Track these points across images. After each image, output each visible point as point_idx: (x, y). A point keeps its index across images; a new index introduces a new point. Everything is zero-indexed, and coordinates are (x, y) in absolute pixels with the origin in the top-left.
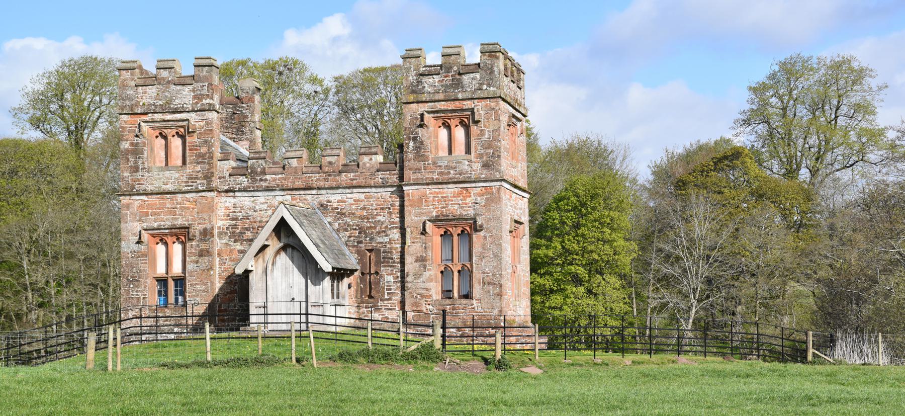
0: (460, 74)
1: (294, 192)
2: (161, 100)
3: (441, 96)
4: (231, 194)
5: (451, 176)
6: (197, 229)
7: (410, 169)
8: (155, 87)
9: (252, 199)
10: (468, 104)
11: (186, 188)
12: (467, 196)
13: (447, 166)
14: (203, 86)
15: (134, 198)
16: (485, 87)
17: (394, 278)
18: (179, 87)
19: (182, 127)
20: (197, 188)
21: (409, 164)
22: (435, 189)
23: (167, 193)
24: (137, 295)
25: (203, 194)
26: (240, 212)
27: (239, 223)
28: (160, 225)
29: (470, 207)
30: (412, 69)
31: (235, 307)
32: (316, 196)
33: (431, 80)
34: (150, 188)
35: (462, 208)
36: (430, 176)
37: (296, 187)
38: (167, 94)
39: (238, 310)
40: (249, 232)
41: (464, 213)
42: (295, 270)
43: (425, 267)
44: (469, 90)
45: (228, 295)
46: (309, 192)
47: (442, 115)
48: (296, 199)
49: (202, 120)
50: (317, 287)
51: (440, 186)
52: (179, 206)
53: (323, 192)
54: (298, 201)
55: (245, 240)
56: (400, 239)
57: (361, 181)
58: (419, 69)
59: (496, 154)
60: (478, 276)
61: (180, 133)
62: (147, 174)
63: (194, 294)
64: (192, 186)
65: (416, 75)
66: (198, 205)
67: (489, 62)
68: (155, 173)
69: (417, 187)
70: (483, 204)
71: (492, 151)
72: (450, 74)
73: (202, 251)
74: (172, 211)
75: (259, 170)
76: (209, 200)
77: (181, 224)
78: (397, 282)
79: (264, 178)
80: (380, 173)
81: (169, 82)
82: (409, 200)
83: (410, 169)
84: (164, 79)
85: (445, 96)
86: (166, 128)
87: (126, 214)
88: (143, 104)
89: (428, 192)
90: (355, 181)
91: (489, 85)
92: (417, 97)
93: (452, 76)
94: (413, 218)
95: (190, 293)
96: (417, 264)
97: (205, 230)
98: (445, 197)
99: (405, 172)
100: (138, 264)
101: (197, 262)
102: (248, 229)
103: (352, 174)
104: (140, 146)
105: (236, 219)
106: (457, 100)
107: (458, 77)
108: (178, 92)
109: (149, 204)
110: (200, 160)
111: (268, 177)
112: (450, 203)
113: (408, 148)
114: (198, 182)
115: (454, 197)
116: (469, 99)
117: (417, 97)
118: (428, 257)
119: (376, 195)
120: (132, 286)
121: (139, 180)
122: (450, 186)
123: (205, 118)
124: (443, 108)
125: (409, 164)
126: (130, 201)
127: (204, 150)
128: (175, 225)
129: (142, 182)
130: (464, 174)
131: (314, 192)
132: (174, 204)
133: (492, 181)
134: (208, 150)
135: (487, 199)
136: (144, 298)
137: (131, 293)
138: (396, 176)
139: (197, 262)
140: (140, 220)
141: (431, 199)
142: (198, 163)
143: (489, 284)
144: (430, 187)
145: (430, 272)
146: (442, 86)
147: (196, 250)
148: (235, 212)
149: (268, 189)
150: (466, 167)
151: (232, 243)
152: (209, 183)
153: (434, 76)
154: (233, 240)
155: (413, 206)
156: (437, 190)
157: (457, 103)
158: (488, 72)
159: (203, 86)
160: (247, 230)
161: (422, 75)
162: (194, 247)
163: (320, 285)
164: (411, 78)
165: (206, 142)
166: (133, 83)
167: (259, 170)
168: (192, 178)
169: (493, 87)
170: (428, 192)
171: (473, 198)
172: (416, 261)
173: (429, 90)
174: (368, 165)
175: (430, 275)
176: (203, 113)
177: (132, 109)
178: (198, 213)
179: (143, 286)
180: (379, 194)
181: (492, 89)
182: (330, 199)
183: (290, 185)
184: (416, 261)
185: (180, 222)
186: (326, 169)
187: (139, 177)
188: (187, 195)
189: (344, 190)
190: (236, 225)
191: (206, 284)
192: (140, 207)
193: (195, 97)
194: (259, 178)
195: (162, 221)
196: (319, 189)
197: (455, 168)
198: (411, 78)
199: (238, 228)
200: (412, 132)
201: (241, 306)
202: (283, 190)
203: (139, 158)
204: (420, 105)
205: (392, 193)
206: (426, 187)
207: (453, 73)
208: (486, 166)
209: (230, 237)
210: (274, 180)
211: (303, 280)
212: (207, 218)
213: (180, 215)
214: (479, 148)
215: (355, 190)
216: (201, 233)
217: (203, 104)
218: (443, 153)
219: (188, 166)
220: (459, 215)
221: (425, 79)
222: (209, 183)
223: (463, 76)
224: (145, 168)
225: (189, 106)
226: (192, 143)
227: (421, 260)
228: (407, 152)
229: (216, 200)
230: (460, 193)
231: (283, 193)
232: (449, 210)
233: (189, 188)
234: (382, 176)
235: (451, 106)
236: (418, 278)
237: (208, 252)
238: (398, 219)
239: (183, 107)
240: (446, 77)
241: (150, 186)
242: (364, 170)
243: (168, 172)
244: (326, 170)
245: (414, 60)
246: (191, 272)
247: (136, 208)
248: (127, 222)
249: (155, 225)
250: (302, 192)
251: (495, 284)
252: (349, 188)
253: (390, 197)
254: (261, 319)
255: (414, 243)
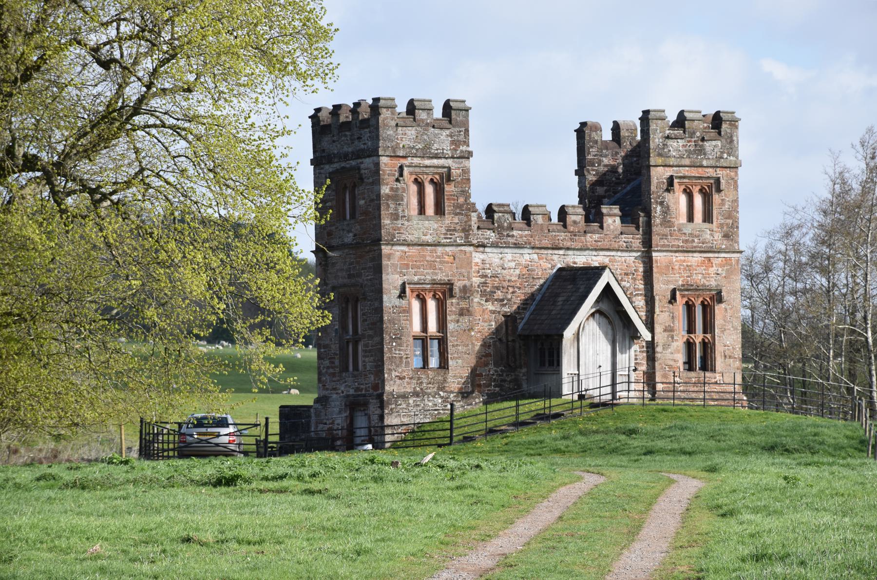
0: (703, 140)
1: (543, 251)
2: (419, 143)
3: (687, 162)
4: (481, 249)
5: (695, 244)
6: (458, 285)
7: (658, 235)
8: (414, 128)
9: (500, 256)
10: (711, 172)
11: (445, 241)
12: (709, 267)
13: (691, 234)
14: (460, 131)
15: (395, 248)
16: (725, 156)
17: (640, 347)
18: (437, 131)
19: (436, 173)
20: (455, 241)
21: (657, 229)
22: (681, 256)
23: (429, 245)
24: (399, 354)
25: (463, 248)
26: (490, 269)
27: (489, 280)
28: (420, 280)
29: (712, 277)
30: (658, 131)
31: (489, 371)
32: (563, 257)
33: (675, 144)
34: (410, 238)
35: (705, 278)
36: (676, 243)
37: (543, 246)
38: (425, 137)
39: (493, 375)
40: (499, 292)
41: (707, 283)
42: (602, 336)
43: (672, 337)
44: (711, 157)
45: (483, 359)
46: (556, 252)
47: (687, 181)
48: (542, 259)
49: (459, 169)
50: (624, 355)
51: (686, 254)
52: (438, 260)
53: (570, 252)
54: (545, 260)
55: (496, 300)
56: (644, 307)
57: (606, 244)
58: (664, 132)
59: (735, 224)
60: (720, 349)
61: (435, 180)
62: (406, 223)
63: (456, 355)
64: (451, 238)
65: (662, 137)
66: (457, 259)
67: (729, 131)
68: (415, 222)
69: (665, 254)
70: (724, 275)
71: (731, 221)
72: (693, 140)
73: (462, 309)
74: (432, 265)
75: (506, 224)
76: (468, 255)
77: (441, 280)
78: (643, 352)
79: (511, 233)
80: (623, 236)
81: (427, 124)
82: (657, 267)
83: (657, 234)
84: (423, 120)
85: (691, 162)
86: (423, 173)
87: (387, 265)
88: (403, 146)
89: (674, 260)
90: (600, 243)
91: (729, 154)
92: (665, 161)
93: (695, 141)
94: (661, 288)
95: (452, 354)
96: (666, 334)
97: (465, 287)
98: (690, 266)
99: (653, 238)
100: (400, 321)
101: (458, 321)
102: (498, 288)
103: (597, 235)
104: (400, 192)
105: (486, 276)
106: (702, 166)
107: (701, 143)
108: (436, 135)
109: (410, 256)
110: (458, 211)
111: (515, 233)
112: (695, 272)
113: (656, 213)
114: (457, 234)
115: (698, 266)
116: (711, 167)
117: (665, 161)
118: (676, 328)
119: (620, 259)
120: (394, 344)
121: (399, 229)
122: (695, 255)
123: (462, 165)
124: (687, 174)
125: (657, 229)
126: (391, 252)
127: (461, 200)
128: (434, 280)
129: (402, 231)
130: (707, 243)
131: (561, 252)
132: (433, 257)
133: (734, 252)
134: (466, 201)
135: (727, 270)
136: (407, 358)
137: (394, 351)
138: (639, 241)
139: (458, 321)
140: (401, 272)
141: (677, 267)
142: (456, 215)
143: (730, 357)
144: (677, 254)
145: (677, 343)
146: (686, 151)
147: (456, 308)
148: (484, 269)
149: (517, 246)
150: (708, 236)
151: (483, 302)
152: (467, 237)
153: (679, 140)
154: (484, 299)
155: (661, 273)
156: (683, 258)
157: (700, 170)
158: (728, 141)
159: (460, 131)
160: (498, 289)
161: (668, 137)
162: (454, 304)
163: (626, 353)
164: (657, 140)
165: (463, 191)
166: (393, 123)
167: (506, 224)
168: (450, 230)
169: (733, 156)
170: (674, 260)
171: (715, 268)
172: (665, 331)
173: (674, 154)
174: (612, 227)
175: (678, 346)
176: (461, 160)
177: (394, 152)
178: (457, 268)
179: (405, 345)
180: (623, 258)
181: (732, 158)
182: (576, 260)
183: (537, 244)
184: (665, 331)
185: (440, 277)
186: (572, 229)
187: (400, 226)
188: (448, 249)
189: (591, 252)
190: (486, 283)
191: (468, 345)
192: (401, 258)
193: (452, 143)
194: (505, 234)
195: (422, 275)
196: (568, 249)
197: (698, 236)
198: (657, 140)
199: (488, 287)
200: (659, 197)
201: (496, 371)
202: (533, 248)
203: (399, 204)
204: (667, 169)
205: (636, 259)
206: (673, 254)
207: (695, 139)
208: (726, 236)
209: (481, 296)
210: (521, 237)
211: (608, 349)
212: (466, 274)
213: (440, 269)
214: (720, 218)
215: (601, 253)
216: (460, 291)
217: (462, 151)
218: (683, 219)
219: (446, 216)
220: (702, 285)
221: (670, 142)
222: (467, 237)
223: (705, 143)
224: (405, 216)
225: (449, 152)
226: (449, 192)
227: (669, 330)
228: (655, 217)
229: (474, 254)
230: (703, 262)
231: (530, 251)
232: (694, 279)
233: (448, 241)
234: (626, 240)
235: (694, 172)
236: (667, 348)
237: (468, 311)
238: (643, 286)
239: (443, 153)
240: (689, 142)
241: (410, 236)
242: (608, 233)
243: (427, 222)
244: (572, 230)
245: (660, 122)
246: (453, 332)
247: (397, 259)
248: (388, 274)
249: (416, 279)
250: (550, 252)
251: (735, 358)
252: (596, 250)
253: (634, 262)
254: (625, 394)
255: (662, 312)
